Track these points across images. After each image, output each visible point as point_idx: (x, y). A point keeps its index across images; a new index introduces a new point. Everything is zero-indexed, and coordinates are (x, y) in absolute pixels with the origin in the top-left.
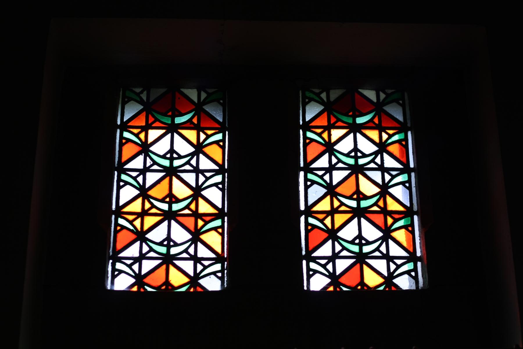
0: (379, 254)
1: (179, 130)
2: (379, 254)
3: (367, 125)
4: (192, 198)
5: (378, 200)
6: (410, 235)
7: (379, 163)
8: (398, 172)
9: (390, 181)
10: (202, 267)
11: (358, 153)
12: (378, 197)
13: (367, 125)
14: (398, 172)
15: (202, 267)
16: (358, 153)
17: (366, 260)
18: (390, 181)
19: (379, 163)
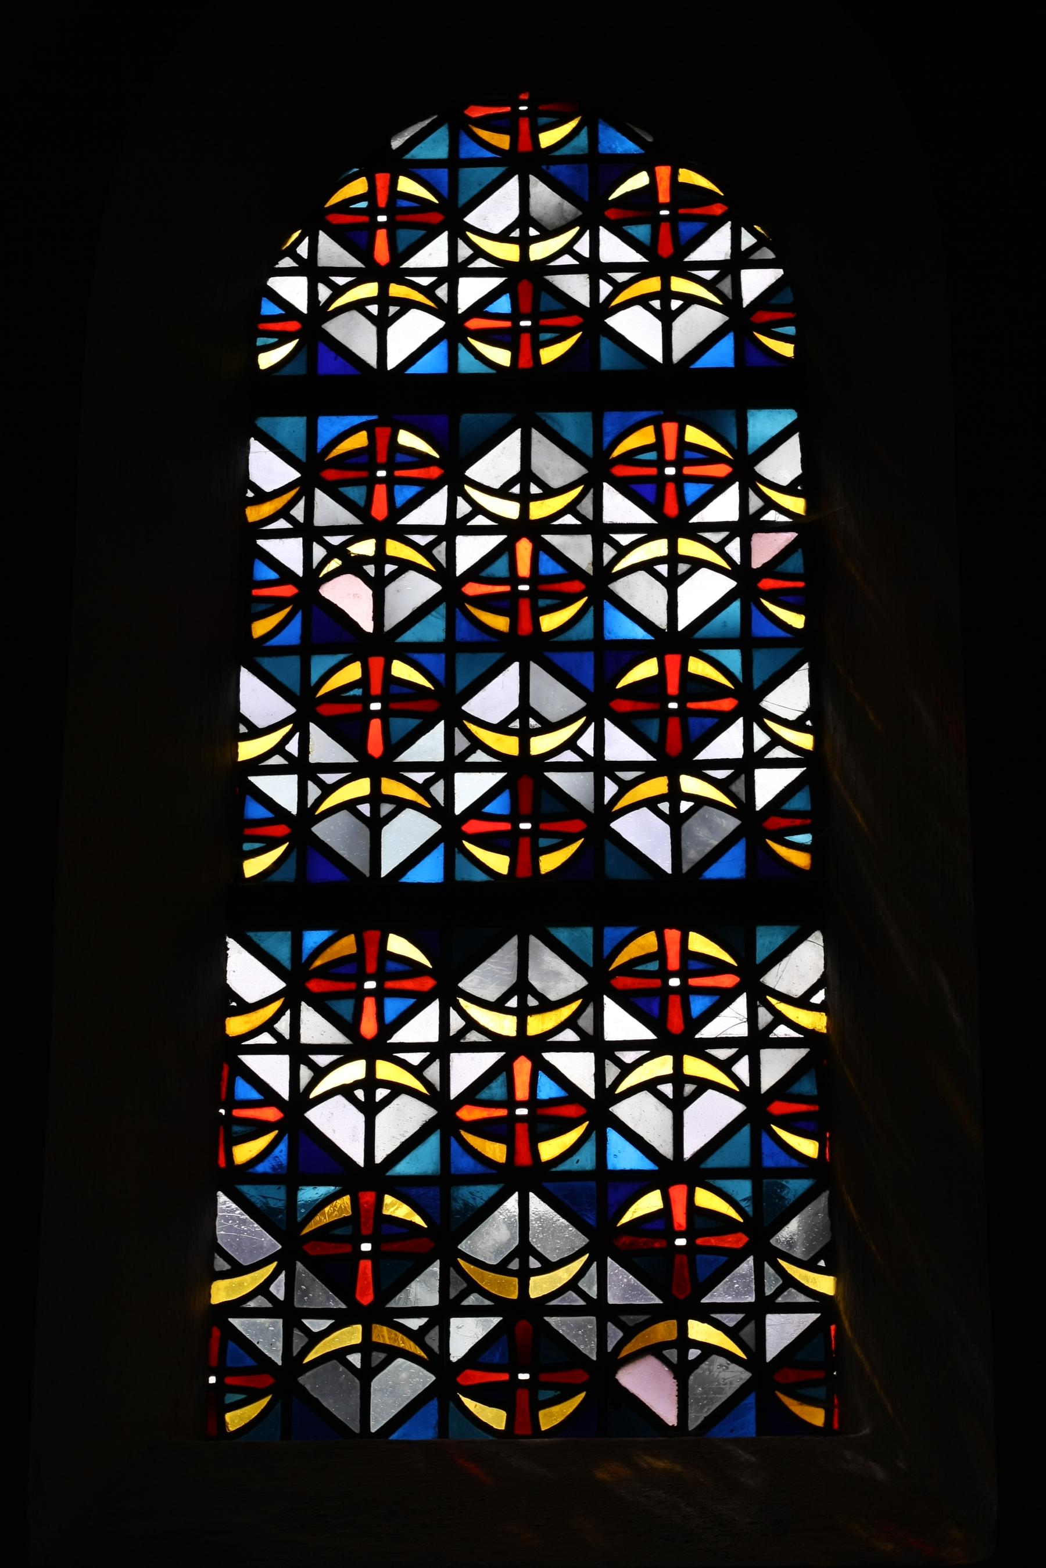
0: (575, 758)
1: (436, 536)
2: (575, 758)
3: (642, 1318)
4: (433, 689)
5: (615, 560)
6: (515, 1240)
7: (311, 785)
8: (552, 264)
9: (331, 300)
10: (577, 247)
11: (368, 814)
12: (313, 1095)
13: (642, 1318)
14: (552, 264)
15: (577, 247)
16: (368, 814)
17: (506, 773)
18: (331, 300)
19: (311, 785)
